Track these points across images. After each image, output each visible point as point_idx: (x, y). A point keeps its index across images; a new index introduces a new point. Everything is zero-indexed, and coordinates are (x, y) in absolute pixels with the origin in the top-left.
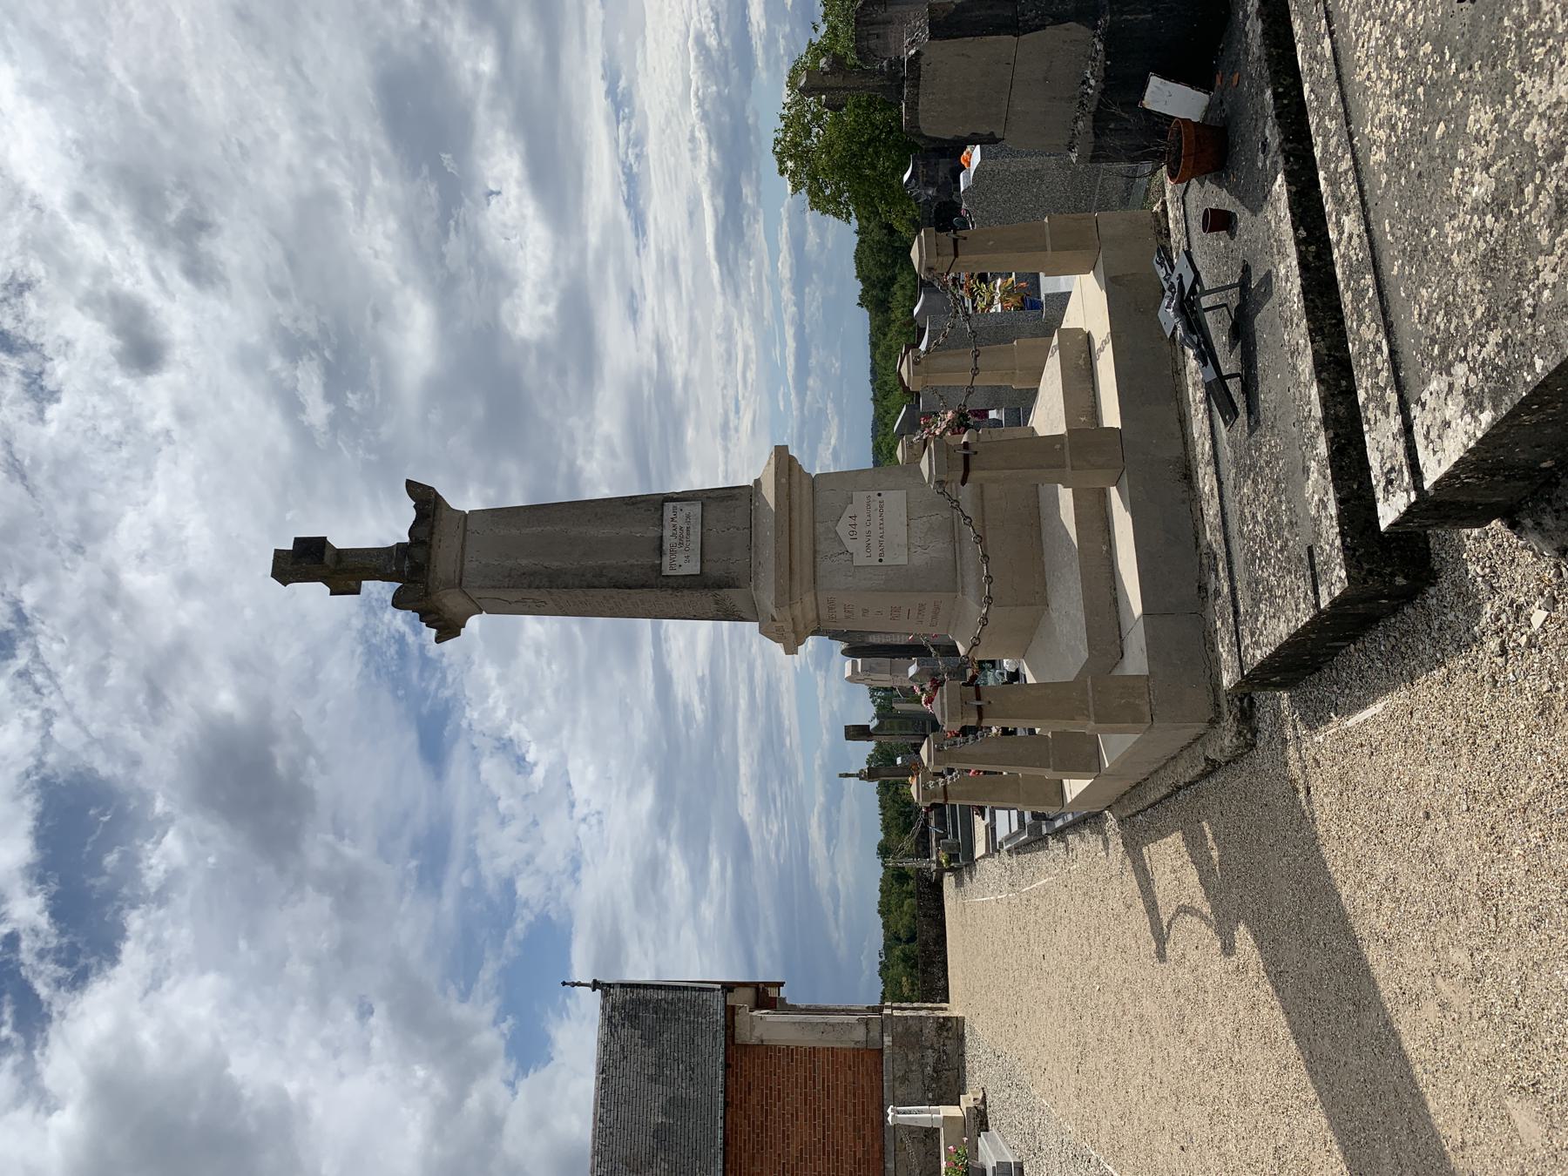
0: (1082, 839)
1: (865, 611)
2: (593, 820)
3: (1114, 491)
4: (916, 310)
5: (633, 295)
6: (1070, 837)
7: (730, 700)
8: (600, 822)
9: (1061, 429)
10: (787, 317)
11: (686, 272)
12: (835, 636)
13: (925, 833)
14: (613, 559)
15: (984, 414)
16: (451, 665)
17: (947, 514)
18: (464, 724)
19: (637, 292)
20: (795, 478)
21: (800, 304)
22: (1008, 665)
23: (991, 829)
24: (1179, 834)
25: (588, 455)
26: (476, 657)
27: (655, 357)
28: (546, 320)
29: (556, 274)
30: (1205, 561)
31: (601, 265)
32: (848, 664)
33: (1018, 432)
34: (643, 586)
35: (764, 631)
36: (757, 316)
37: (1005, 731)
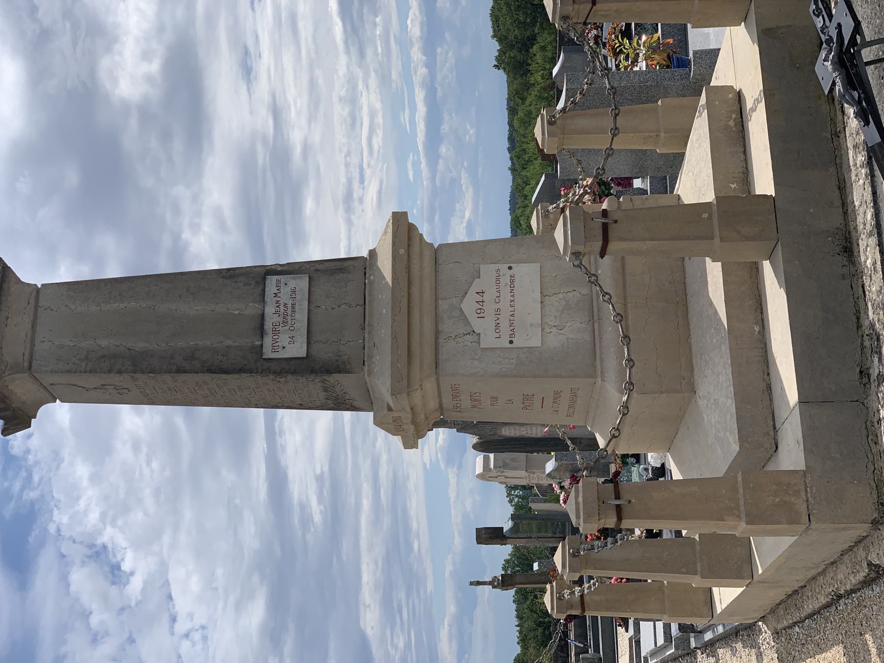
0: (734, 652)
1: (494, 399)
2: (197, 636)
3: (767, 265)
4: (555, 71)
5: (246, 52)
6: (720, 651)
7: (352, 500)
8: (205, 638)
9: (709, 196)
10: (417, 79)
11: (305, 28)
12: (464, 427)
13: (564, 647)
14: (214, 340)
15: (625, 182)
16: (37, 463)
17: (585, 291)
18: (52, 528)
19: (252, 49)
20: (416, 249)
21: (431, 64)
22: (653, 459)
23: (636, 642)
24: (840, 648)
25: (196, 228)
26: (66, 453)
27: (271, 122)
28: (149, 79)
29: (161, 29)
30: (867, 343)
31: (211, 20)
32: (480, 458)
33: (664, 200)
34: (241, 371)
35: (378, 423)
36: (384, 78)
37: (650, 534)
